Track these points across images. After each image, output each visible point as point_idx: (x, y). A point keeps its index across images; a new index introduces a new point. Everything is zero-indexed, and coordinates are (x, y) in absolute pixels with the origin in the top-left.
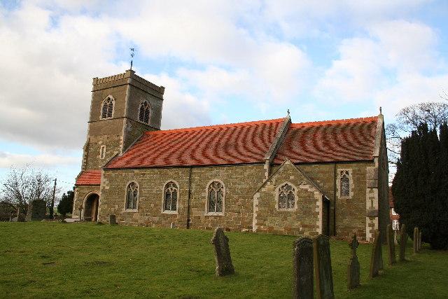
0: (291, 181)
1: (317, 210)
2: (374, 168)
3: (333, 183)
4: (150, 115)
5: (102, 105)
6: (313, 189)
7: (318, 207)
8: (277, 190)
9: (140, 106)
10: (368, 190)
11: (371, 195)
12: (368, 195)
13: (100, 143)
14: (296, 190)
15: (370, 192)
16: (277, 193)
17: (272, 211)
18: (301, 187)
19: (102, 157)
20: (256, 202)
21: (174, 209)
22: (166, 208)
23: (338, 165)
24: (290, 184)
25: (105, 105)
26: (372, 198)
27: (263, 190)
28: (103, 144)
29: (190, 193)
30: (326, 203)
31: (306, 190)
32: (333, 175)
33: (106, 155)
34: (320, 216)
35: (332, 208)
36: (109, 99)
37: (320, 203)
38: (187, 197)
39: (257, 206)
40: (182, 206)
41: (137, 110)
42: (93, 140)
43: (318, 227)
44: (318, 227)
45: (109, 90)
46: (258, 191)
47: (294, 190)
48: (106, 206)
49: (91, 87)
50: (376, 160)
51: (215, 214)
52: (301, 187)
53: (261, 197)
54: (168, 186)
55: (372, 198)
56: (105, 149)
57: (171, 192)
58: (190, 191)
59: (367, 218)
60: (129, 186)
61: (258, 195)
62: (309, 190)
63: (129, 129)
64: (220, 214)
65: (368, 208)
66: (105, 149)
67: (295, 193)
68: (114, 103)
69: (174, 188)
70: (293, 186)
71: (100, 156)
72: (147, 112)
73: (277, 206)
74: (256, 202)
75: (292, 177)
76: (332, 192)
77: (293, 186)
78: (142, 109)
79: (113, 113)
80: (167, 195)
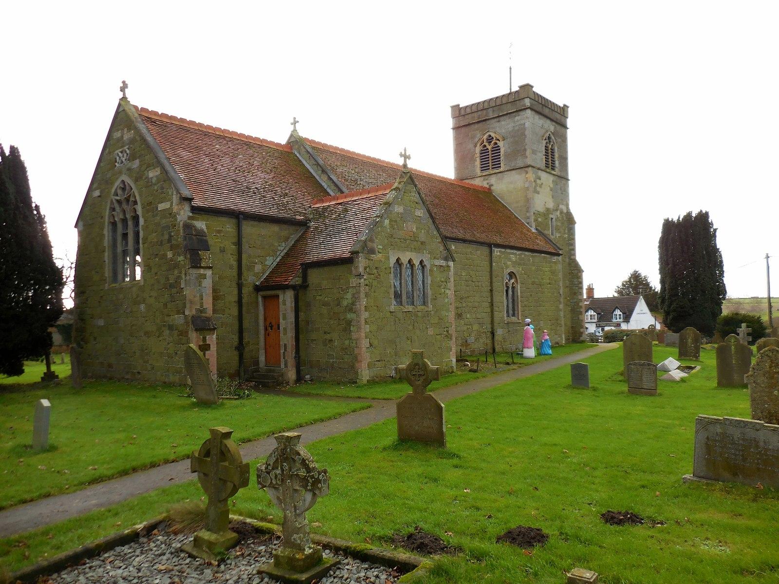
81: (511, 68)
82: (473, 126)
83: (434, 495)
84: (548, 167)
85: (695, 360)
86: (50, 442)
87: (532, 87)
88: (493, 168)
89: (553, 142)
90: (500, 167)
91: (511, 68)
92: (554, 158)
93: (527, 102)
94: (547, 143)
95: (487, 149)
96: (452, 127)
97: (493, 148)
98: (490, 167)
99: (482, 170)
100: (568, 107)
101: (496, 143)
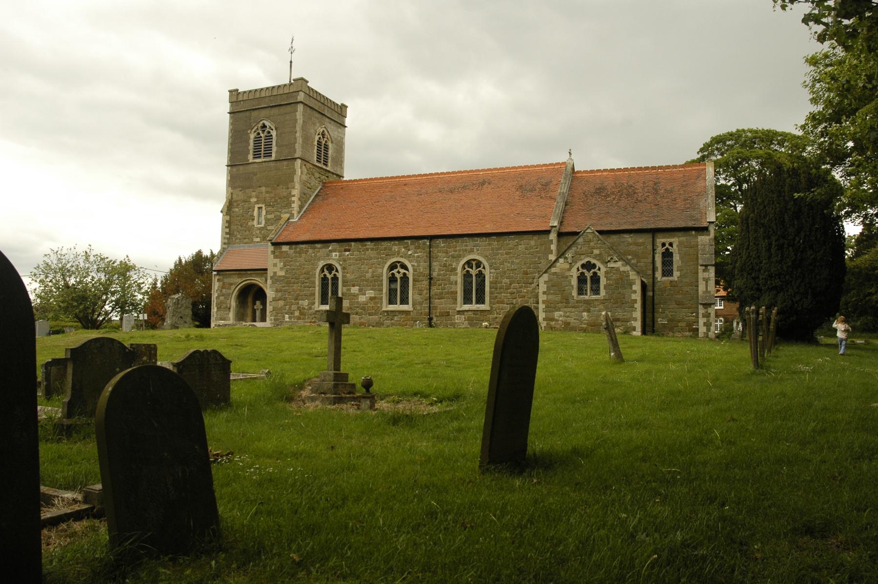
0: (595, 257)
1: (634, 297)
2: (708, 238)
3: (650, 260)
4: (330, 152)
5: (252, 136)
6: (628, 268)
7: (635, 292)
8: (574, 270)
9: (317, 138)
10: (701, 268)
11: (706, 275)
12: (701, 275)
13: (254, 200)
14: (603, 269)
15: (704, 271)
16: (574, 274)
17: (566, 300)
18: (611, 265)
19: (259, 223)
20: (543, 288)
21: (404, 301)
22: (391, 301)
23: (658, 235)
24: (593, 261)
25: (258, 140)
26: (706, 280)
27: (553, 270)
28: (257, 202)
29: (431, 279)
30: (644, 286)
31: (618, 269)
32: (650, 247)
33: (267, 220)
34: (638, 306)
35: (650, 294)
36: (264, 126)
37: (637, 287)
38: (426, 283)
39: (544, 293)
40: (418, 298)
41: (313, 145)
42: (239, 195)
43: (635, 319)
44: (635, 319)
45: (264, 113)
46: (546, 272)
47: (599, 269)
48: (281, 303)
49: (227, 107)
50: (712, 229)
51: (474, 306)
52: (611, 265)
53: (550, 280)
54: (393, 267)
55: (706, 280)
56: (264, 212)
57: (398, 276)
58: (430, 275)
59: (700, 307)
60: (322, 270)
61: (545, 277)
62: (622, 269)
63: (304, 177)
64: (481, 307)
65: (700, 293)
66: (264, 212)
67: (601, 274)
68: (274, 133)
69: (402, 271)
70: (598, 264)
71: (255, 223)
72: (326, 148)
73: (575, 293)
74: (543, 288)
75: (596, 252)
76: (650, 272)
77: (598, 264)
78: (319, 143)
79: (274, 149)
80: (392, 280)
81: (291, 62)
82: (314, 112)
83: (832, 79)
84: (320, 162)
85: (752, 139)
86: (273, 247)
87: (307, 82)
88: (265, 156)
89: (327, 139)
90: (271, 156)
91: (291, 62)
92: (327, 154)
93: (301, 97)
94: (320, 138)
95: (261, 137)
96: (229, 111)
97: (256, 138)
98: (262, 155)
99: (254, 158)
100: (347, 107)
101: (269, 132)
